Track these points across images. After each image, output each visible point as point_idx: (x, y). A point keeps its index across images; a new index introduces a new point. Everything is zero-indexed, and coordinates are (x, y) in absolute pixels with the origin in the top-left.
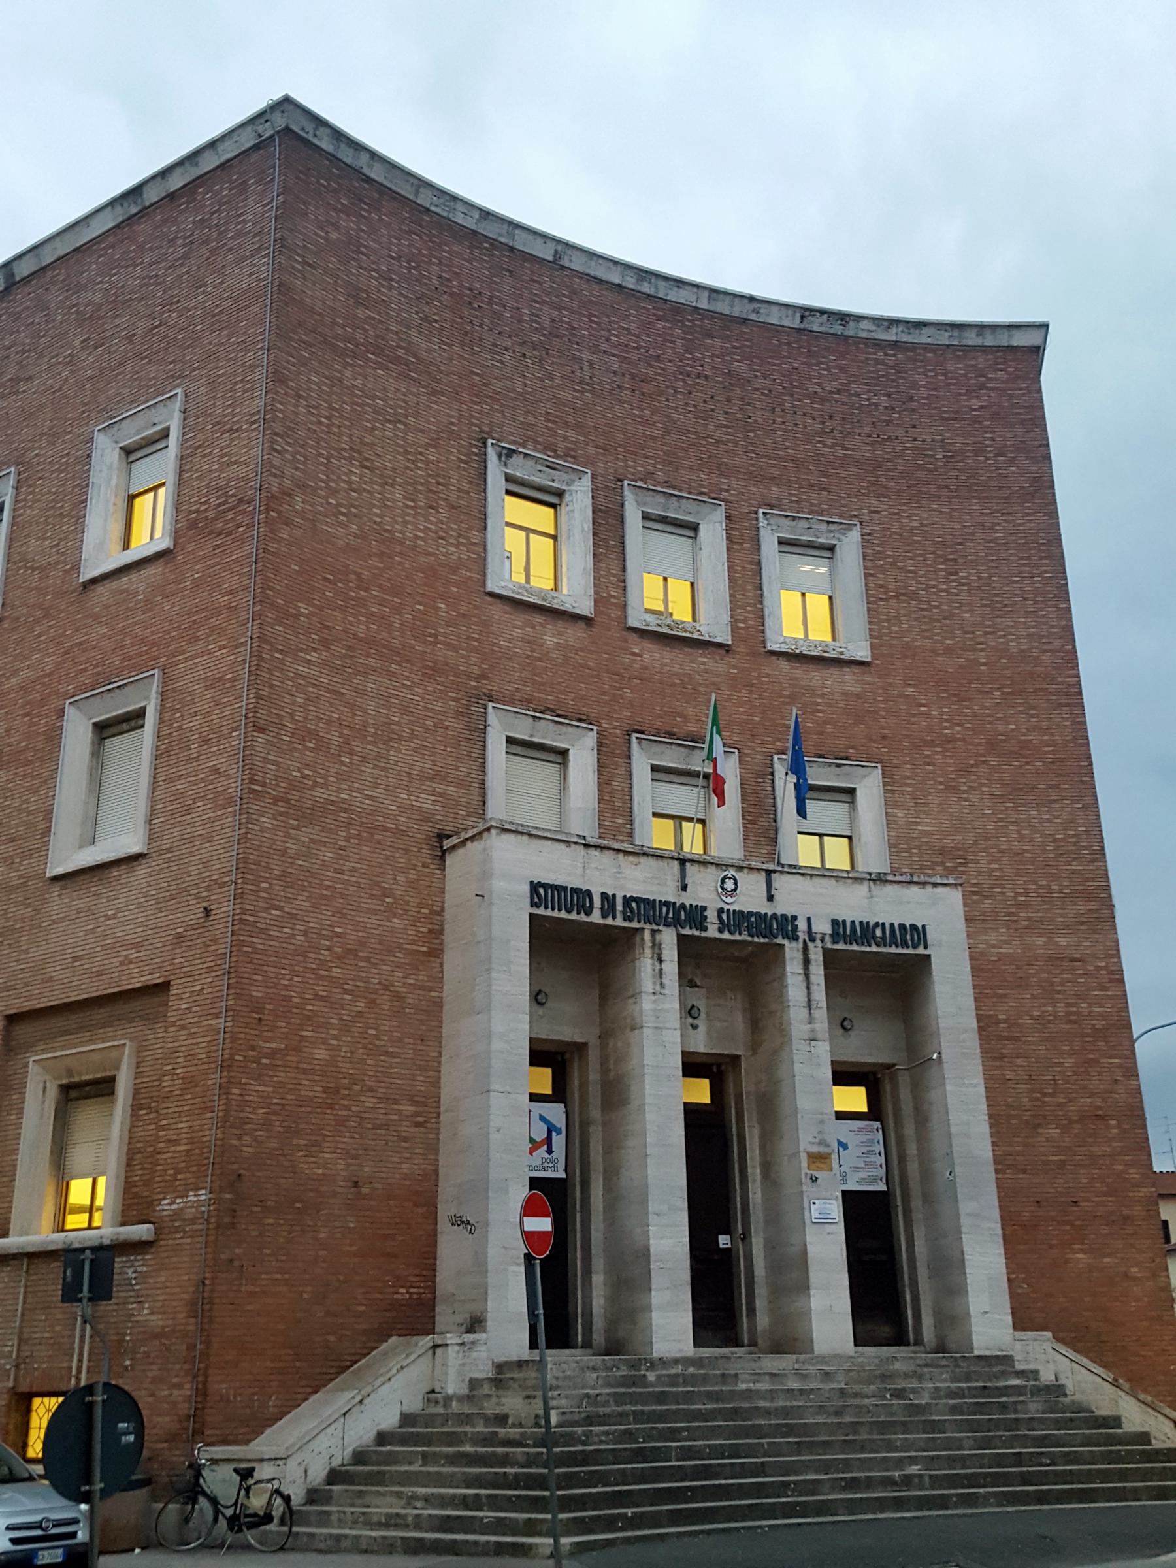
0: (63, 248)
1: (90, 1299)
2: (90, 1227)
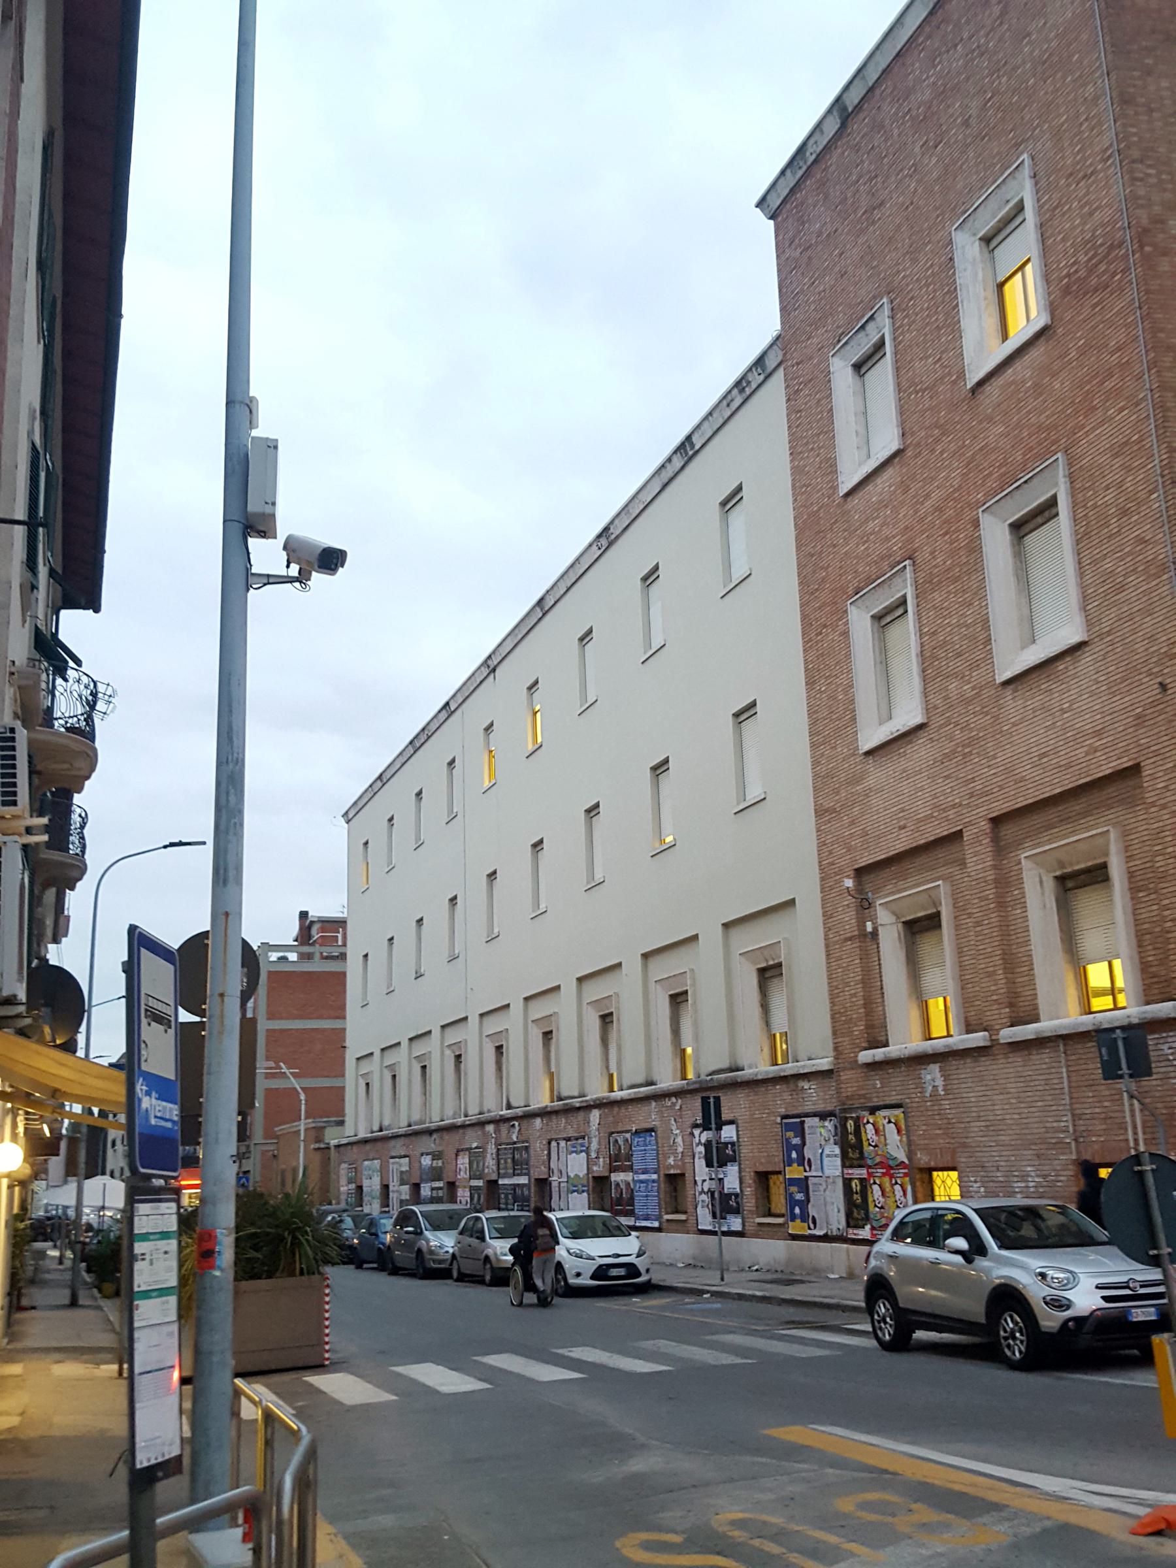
0: (883, 61)
1: (1131, 1076)
2: (1116, 1008)
